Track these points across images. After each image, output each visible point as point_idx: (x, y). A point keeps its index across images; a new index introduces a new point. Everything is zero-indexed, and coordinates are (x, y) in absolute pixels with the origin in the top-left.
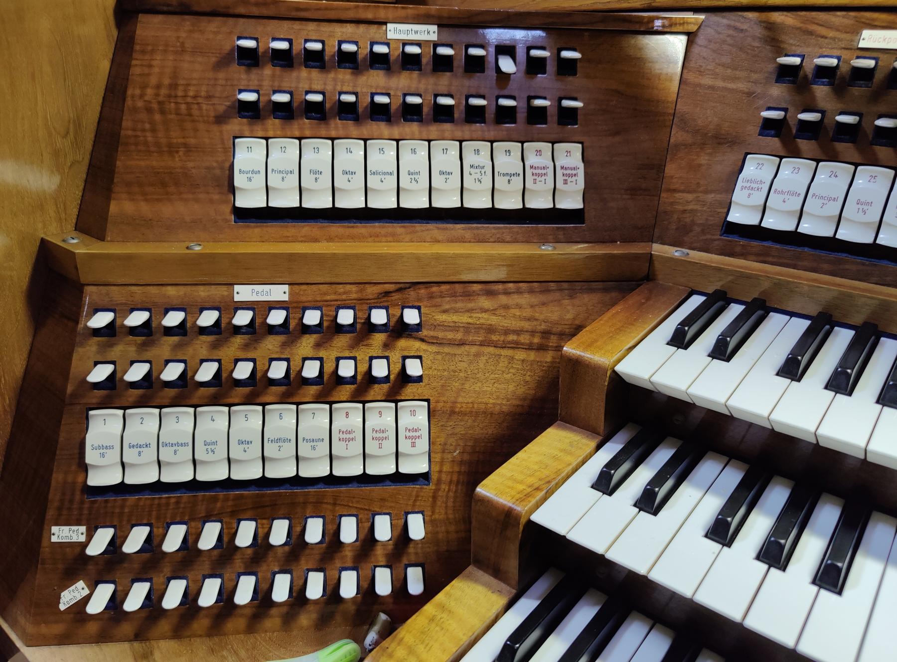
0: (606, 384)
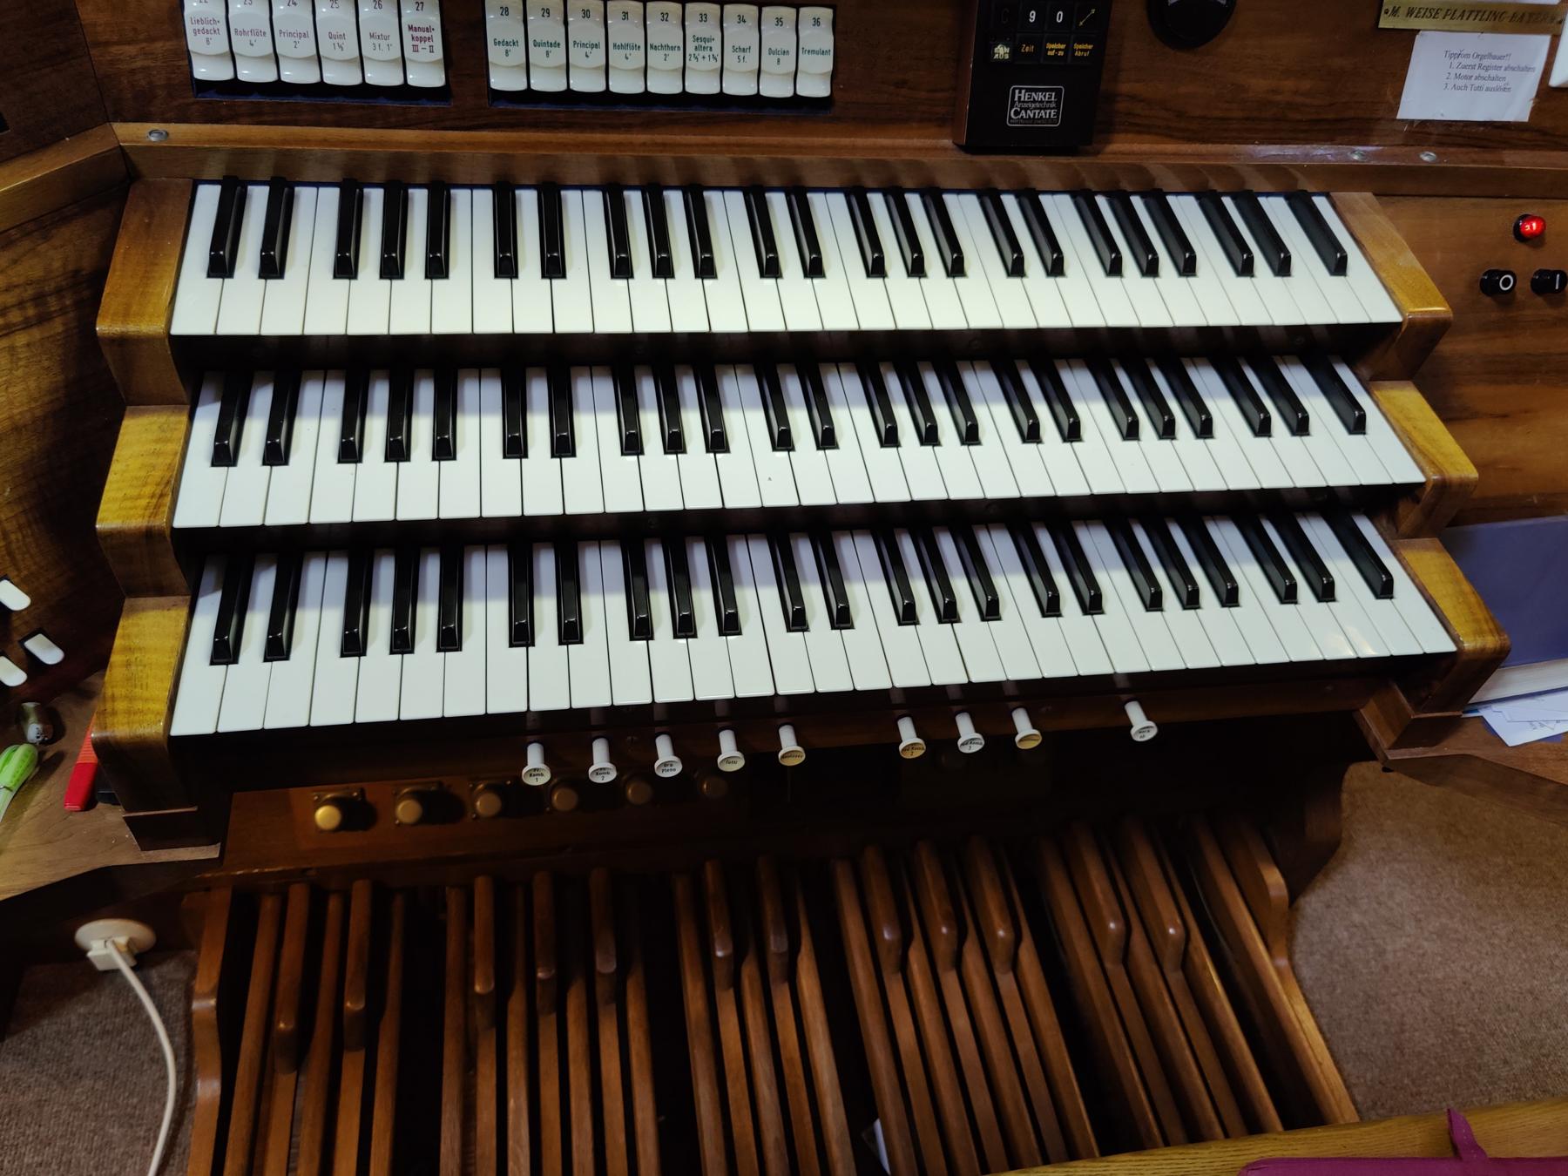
0: (169, 352)
